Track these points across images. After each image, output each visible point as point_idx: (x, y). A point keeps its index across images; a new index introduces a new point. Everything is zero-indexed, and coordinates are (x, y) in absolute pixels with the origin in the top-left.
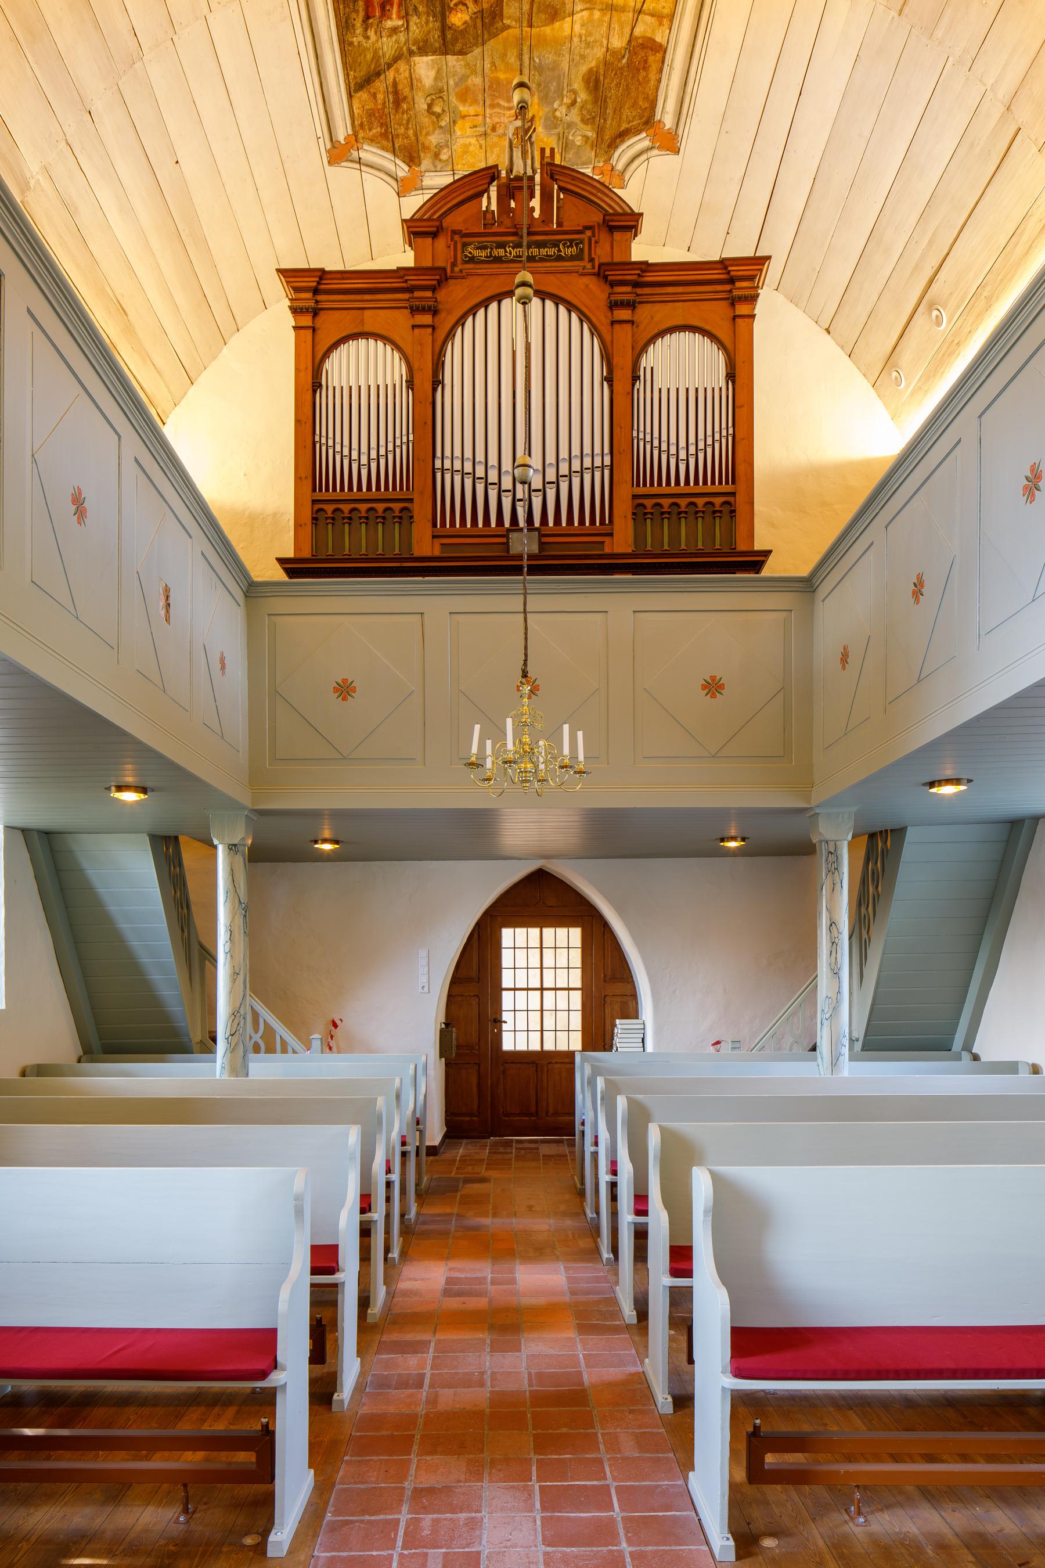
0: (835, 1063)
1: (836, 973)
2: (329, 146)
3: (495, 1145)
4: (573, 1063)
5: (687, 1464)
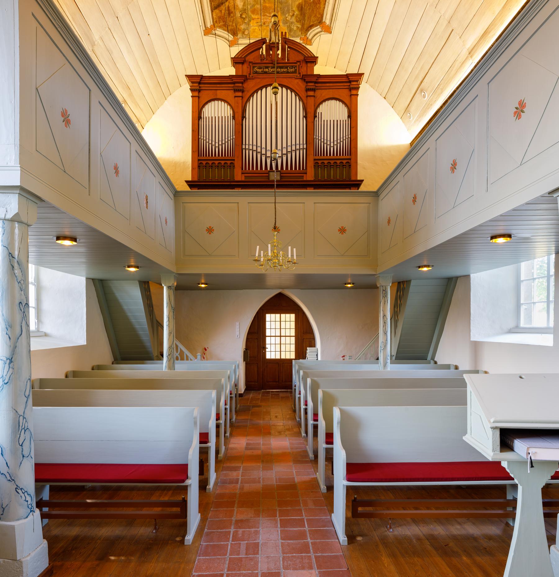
0: (385, 365)
1: (385, 333)
2: (204, 29)
3: (264, 392)
4: (292, 363)
5: (331, 511)
